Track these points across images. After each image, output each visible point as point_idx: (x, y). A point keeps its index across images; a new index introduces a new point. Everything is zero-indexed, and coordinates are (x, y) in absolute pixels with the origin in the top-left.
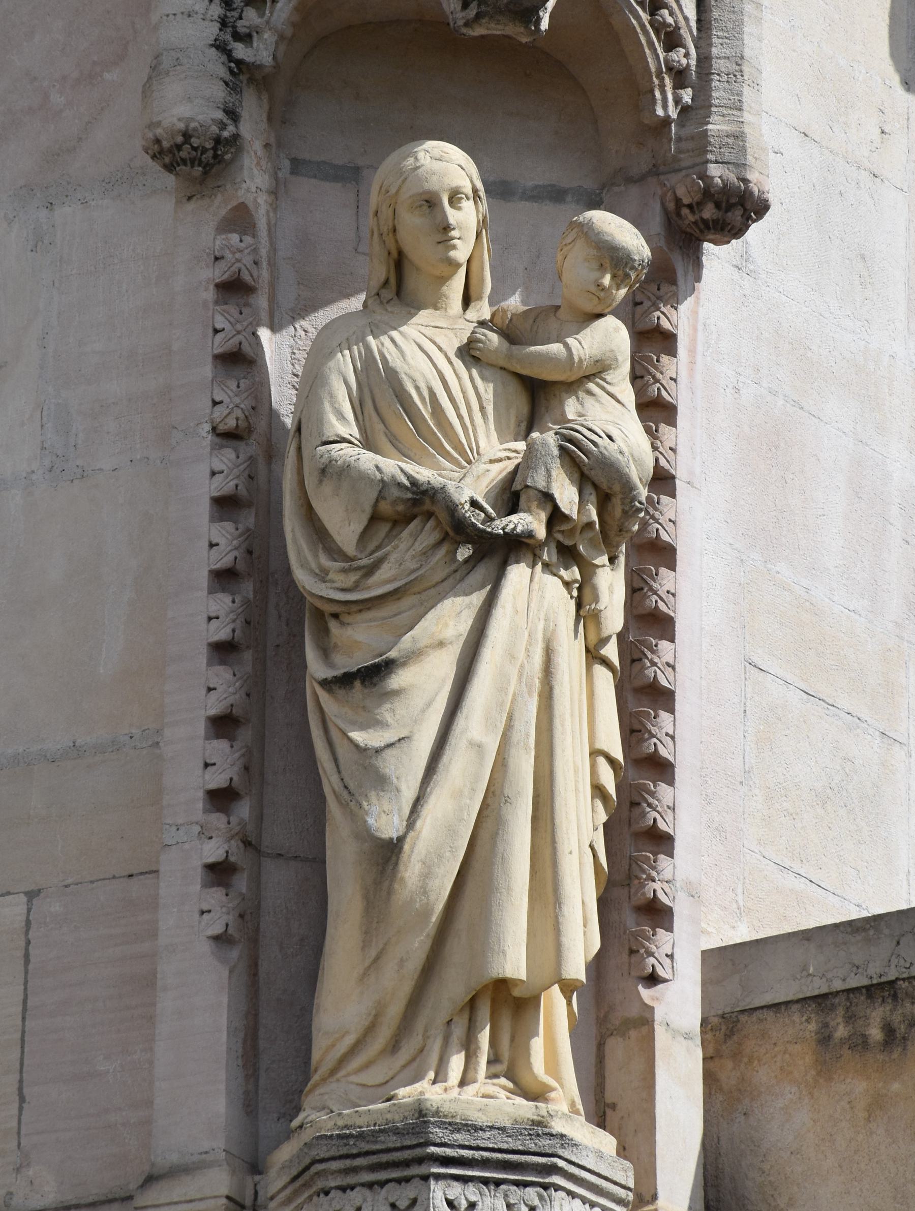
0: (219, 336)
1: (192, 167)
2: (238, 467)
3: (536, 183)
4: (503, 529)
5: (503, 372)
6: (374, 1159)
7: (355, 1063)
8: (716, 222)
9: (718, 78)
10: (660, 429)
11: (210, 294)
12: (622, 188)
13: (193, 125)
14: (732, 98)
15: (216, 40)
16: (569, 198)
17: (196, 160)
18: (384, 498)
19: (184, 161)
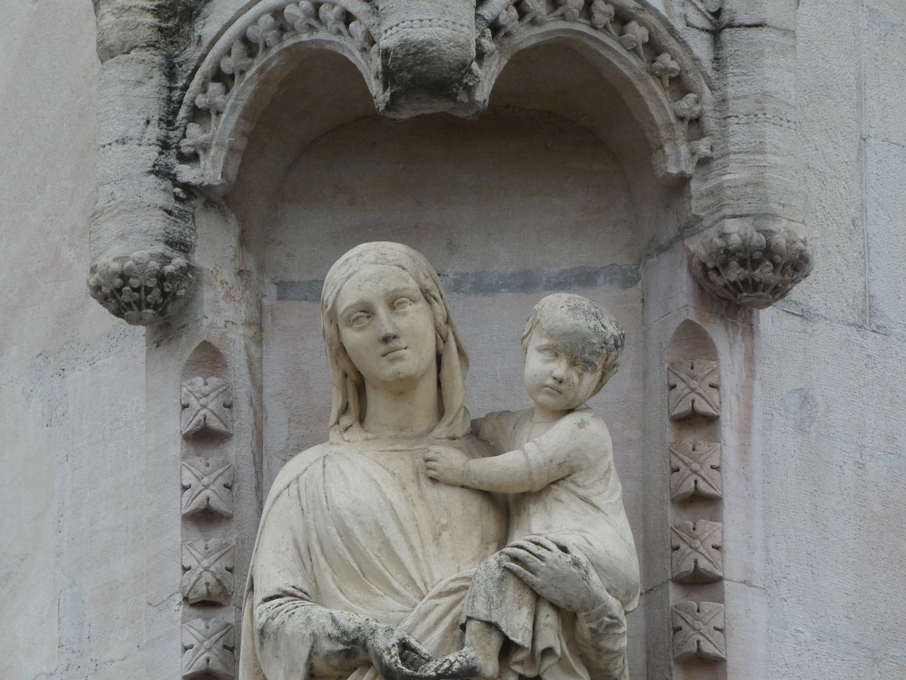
0: (188, 492)
1: (140, 310)
2: (209, 638)
3: (563, 268)
4: (436, 670)
5: (464, 491)
8: (745, 282)
9: (736, 120)
10: (698, 527)
11: (177, 448)
12: (655, 259)
13: (129, 263)
14: (752, 140)
15: (154, 166)
16: (601, 280)
17: (150, 300)
18: (316, 654)
19: (129, 305)
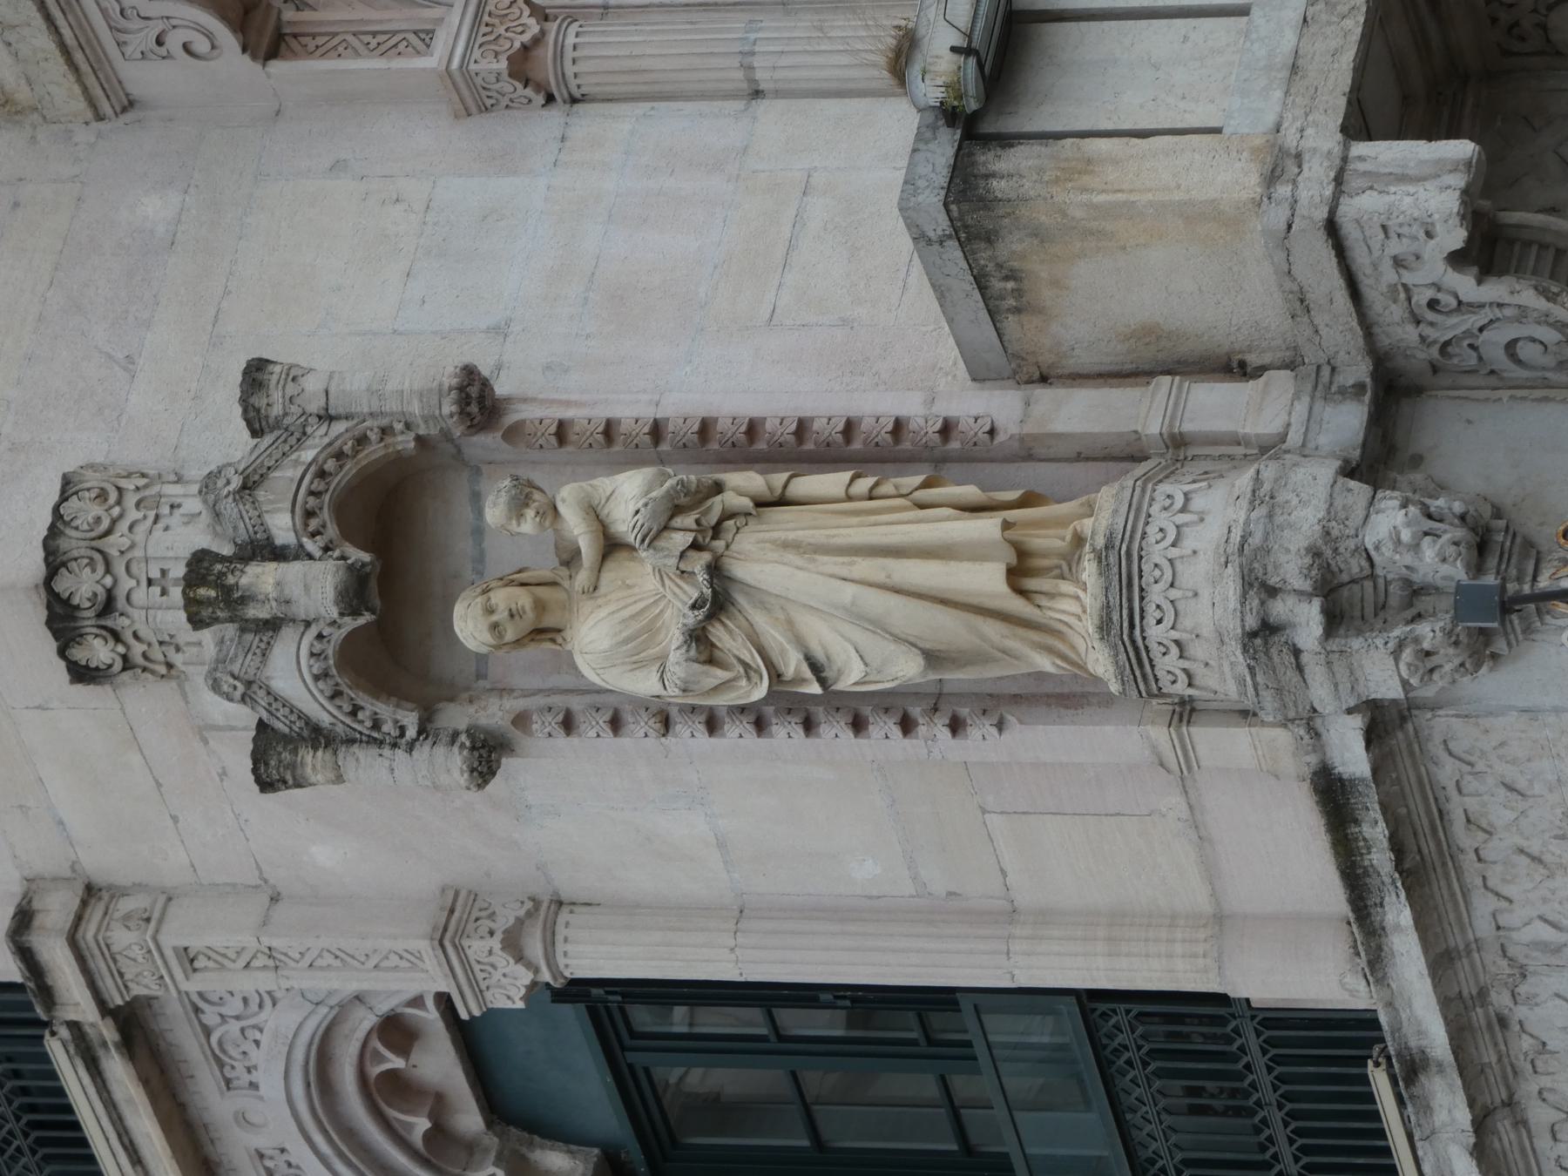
6: (1135, 667)
7: (1073, 656)
17: (487, 755)
